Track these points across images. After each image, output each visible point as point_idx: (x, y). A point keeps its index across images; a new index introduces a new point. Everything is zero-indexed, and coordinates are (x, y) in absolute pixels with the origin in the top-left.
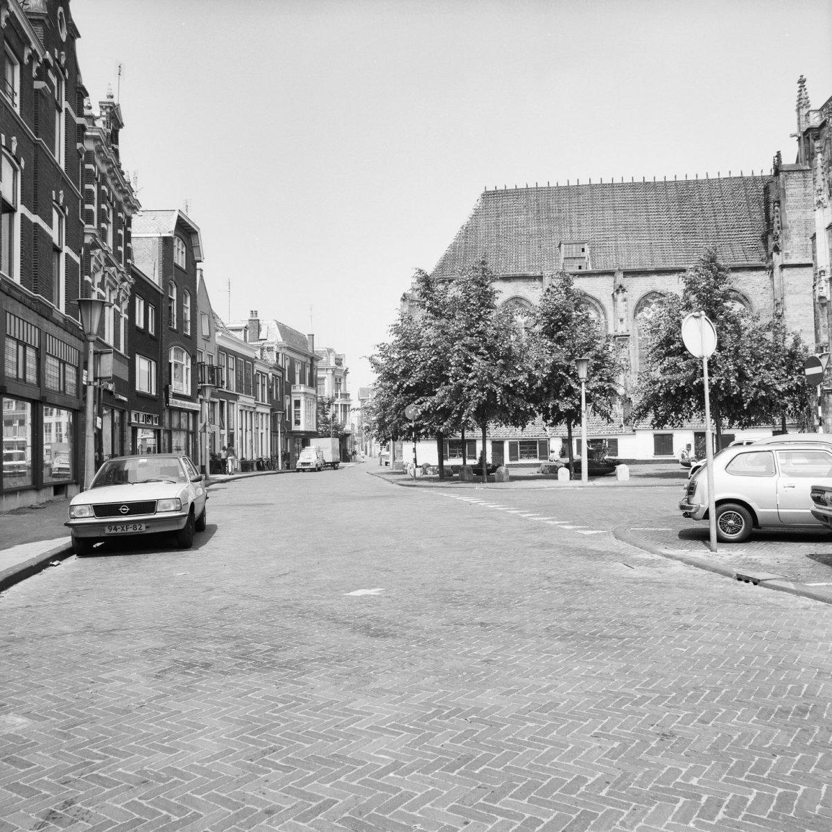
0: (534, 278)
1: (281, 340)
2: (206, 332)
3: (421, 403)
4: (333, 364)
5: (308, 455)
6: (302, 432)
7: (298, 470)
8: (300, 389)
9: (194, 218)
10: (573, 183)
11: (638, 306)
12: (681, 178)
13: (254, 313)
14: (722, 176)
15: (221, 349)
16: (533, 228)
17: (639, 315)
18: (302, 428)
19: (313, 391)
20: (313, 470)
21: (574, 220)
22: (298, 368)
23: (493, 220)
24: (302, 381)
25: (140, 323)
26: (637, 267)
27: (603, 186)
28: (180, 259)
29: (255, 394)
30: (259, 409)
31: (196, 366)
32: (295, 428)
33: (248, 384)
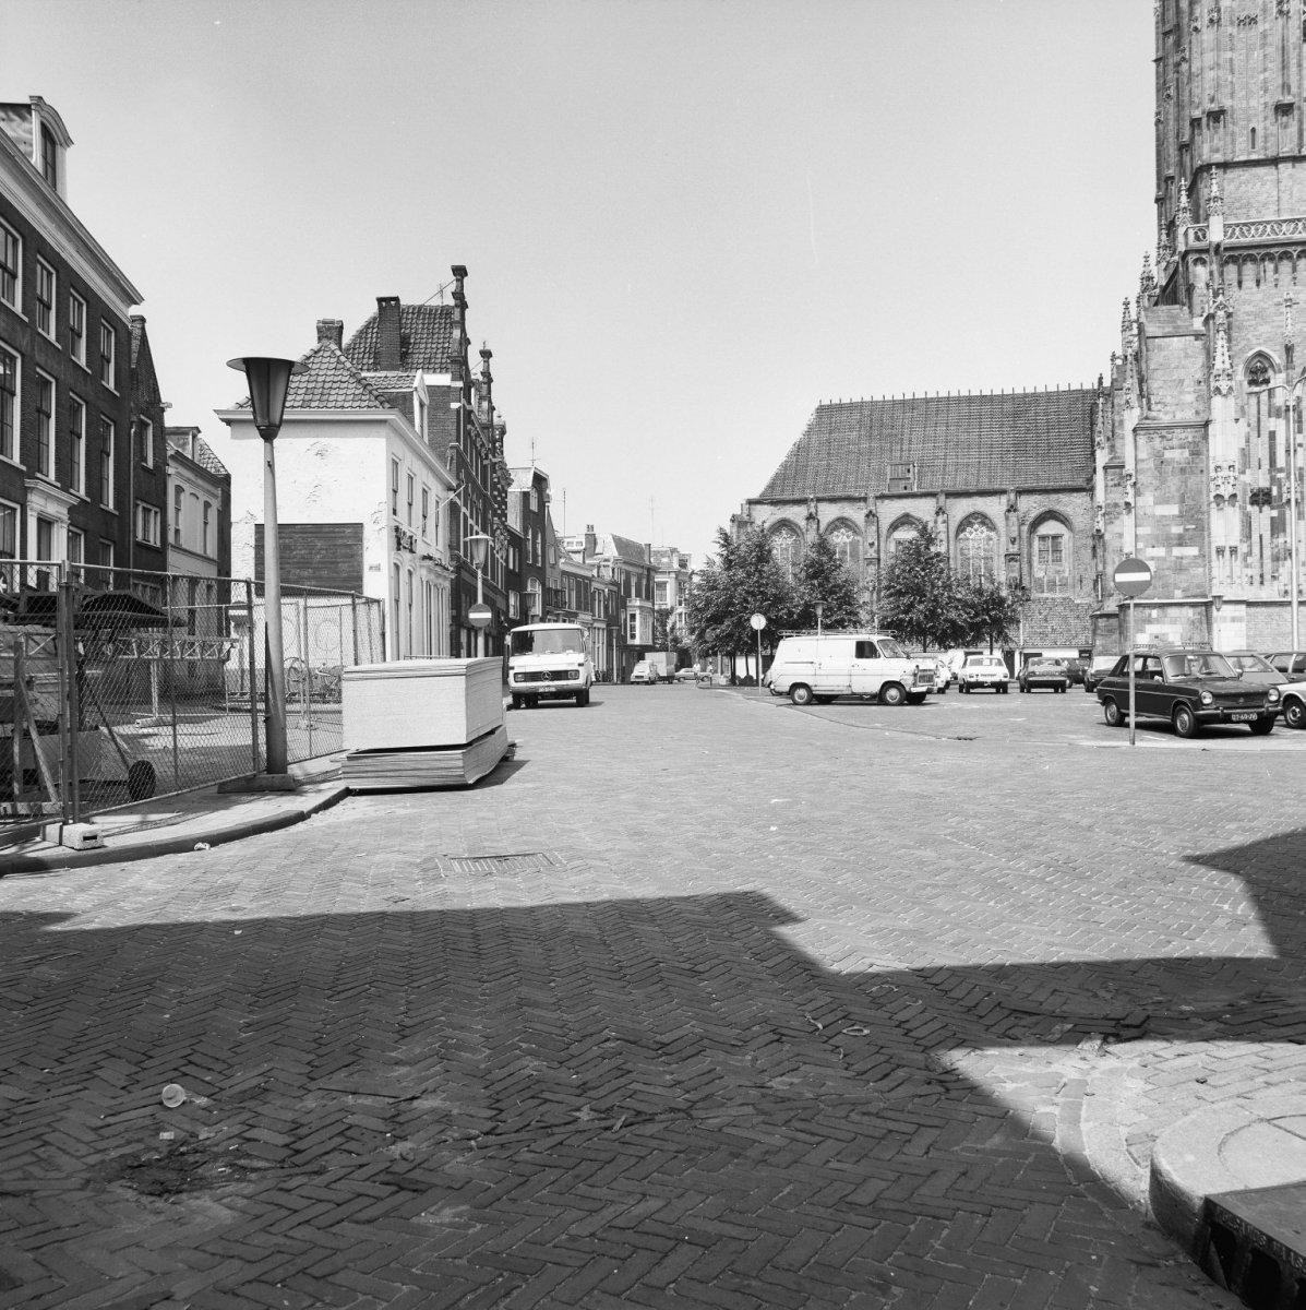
0: (859, 499)
1: (616, 554)
2: (552, 561)
3: (714, 629)
4: (676, 566)
5: (642, 669)
6: (637, 646)
7: (633, 683)
8: (635, 602)
9: (544, 470)
10: (909, 396)
11: (960, 526)
12: (1019, 391)
13: (590, 528)
14: (1061, 389)
15: (564, 573)
16: (865, 445)
17: (962, 536)
18: (637, 641)
19: (649, 605)
20: (647, 683)
21: (906, 437)
22: (634, 581)
23: (825, 437)
24: (638, 595)
25: (511, 567)
26: (960, 487)
27: (939, 400)
28: (534, 507)
29: (593, 611)
30: (596, 625)
31: (546, 591)
32: (630, 642)
33: (586, 603)
